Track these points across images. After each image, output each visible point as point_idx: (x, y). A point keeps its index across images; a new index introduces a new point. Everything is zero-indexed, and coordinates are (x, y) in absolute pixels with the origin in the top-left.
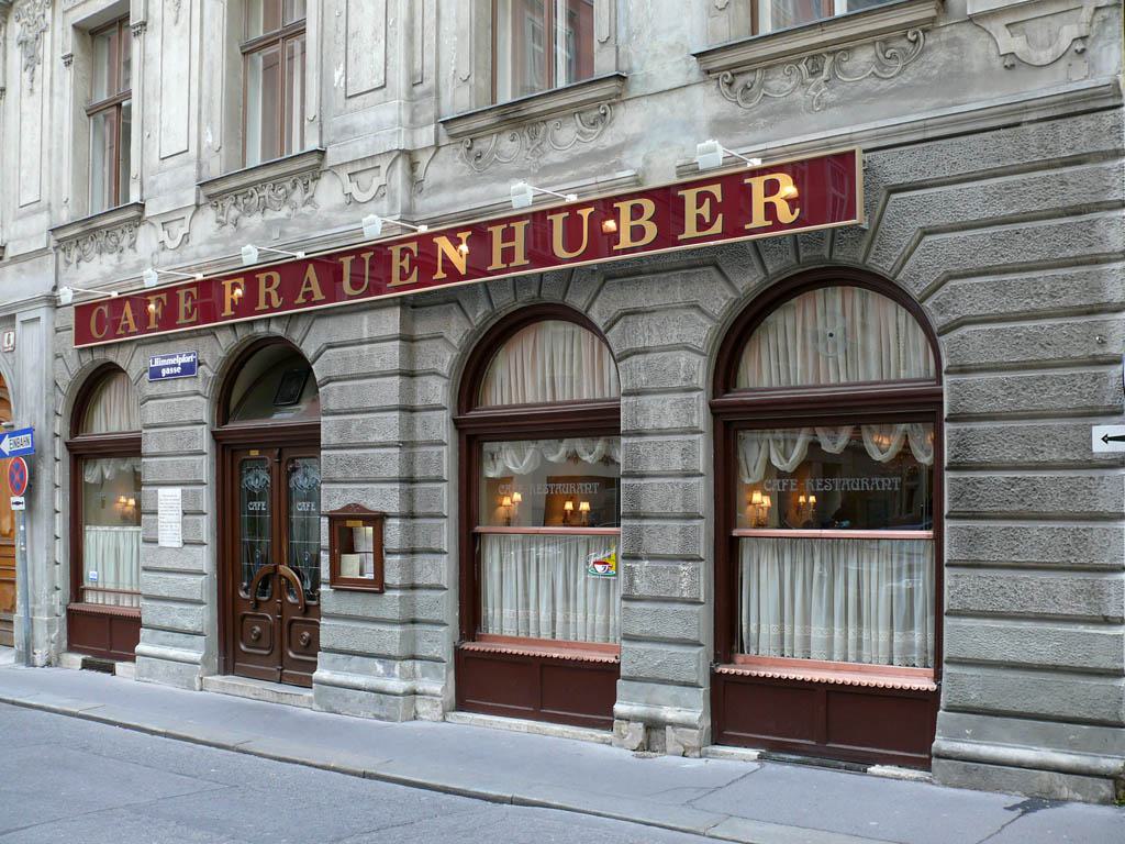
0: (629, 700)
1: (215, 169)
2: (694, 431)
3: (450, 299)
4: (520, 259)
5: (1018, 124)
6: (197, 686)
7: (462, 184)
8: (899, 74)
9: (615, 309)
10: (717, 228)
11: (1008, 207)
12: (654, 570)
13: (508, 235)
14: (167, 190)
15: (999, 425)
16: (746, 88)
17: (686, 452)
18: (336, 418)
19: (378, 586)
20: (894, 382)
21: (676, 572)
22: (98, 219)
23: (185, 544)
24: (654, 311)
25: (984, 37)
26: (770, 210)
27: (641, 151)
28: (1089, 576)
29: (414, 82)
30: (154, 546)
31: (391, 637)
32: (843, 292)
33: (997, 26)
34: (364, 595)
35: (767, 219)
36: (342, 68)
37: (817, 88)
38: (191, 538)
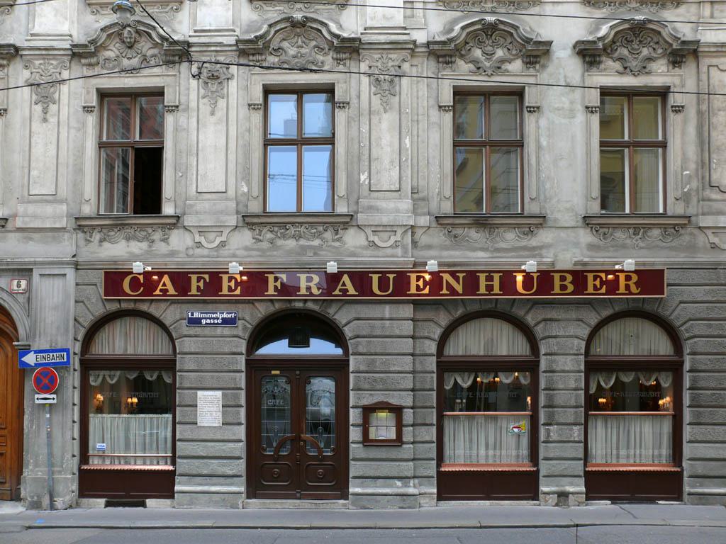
0: (547, 486)
1: (87, 210)
3: (589, 303)
4: (497, 290)
5: (716, 269)
6: (241, 506)
7: (446, 248)
8: (671, 242)
9: (540, 318)
10: (603, 290)
11: (713, 297)
12: (560, 430)
13: (490, 278)
14: (205, 212)
15: (708, 374)
17: (576, 380)
18: (364, 357)
19: (399, 441)
21: (571, 430)
22: (595, 219)
23: (223, 424)
24: (559, 320)
25: (703, 235)
26: (627, 287)
27: (552, 251)
29: (415, 191)
30: (195, 426)
31: (408, 468)
32: (625, 324)
33: (709, 232)
34: (388, 448)
36: (366, 174)
37: (637, 240)
38: (230, 420)
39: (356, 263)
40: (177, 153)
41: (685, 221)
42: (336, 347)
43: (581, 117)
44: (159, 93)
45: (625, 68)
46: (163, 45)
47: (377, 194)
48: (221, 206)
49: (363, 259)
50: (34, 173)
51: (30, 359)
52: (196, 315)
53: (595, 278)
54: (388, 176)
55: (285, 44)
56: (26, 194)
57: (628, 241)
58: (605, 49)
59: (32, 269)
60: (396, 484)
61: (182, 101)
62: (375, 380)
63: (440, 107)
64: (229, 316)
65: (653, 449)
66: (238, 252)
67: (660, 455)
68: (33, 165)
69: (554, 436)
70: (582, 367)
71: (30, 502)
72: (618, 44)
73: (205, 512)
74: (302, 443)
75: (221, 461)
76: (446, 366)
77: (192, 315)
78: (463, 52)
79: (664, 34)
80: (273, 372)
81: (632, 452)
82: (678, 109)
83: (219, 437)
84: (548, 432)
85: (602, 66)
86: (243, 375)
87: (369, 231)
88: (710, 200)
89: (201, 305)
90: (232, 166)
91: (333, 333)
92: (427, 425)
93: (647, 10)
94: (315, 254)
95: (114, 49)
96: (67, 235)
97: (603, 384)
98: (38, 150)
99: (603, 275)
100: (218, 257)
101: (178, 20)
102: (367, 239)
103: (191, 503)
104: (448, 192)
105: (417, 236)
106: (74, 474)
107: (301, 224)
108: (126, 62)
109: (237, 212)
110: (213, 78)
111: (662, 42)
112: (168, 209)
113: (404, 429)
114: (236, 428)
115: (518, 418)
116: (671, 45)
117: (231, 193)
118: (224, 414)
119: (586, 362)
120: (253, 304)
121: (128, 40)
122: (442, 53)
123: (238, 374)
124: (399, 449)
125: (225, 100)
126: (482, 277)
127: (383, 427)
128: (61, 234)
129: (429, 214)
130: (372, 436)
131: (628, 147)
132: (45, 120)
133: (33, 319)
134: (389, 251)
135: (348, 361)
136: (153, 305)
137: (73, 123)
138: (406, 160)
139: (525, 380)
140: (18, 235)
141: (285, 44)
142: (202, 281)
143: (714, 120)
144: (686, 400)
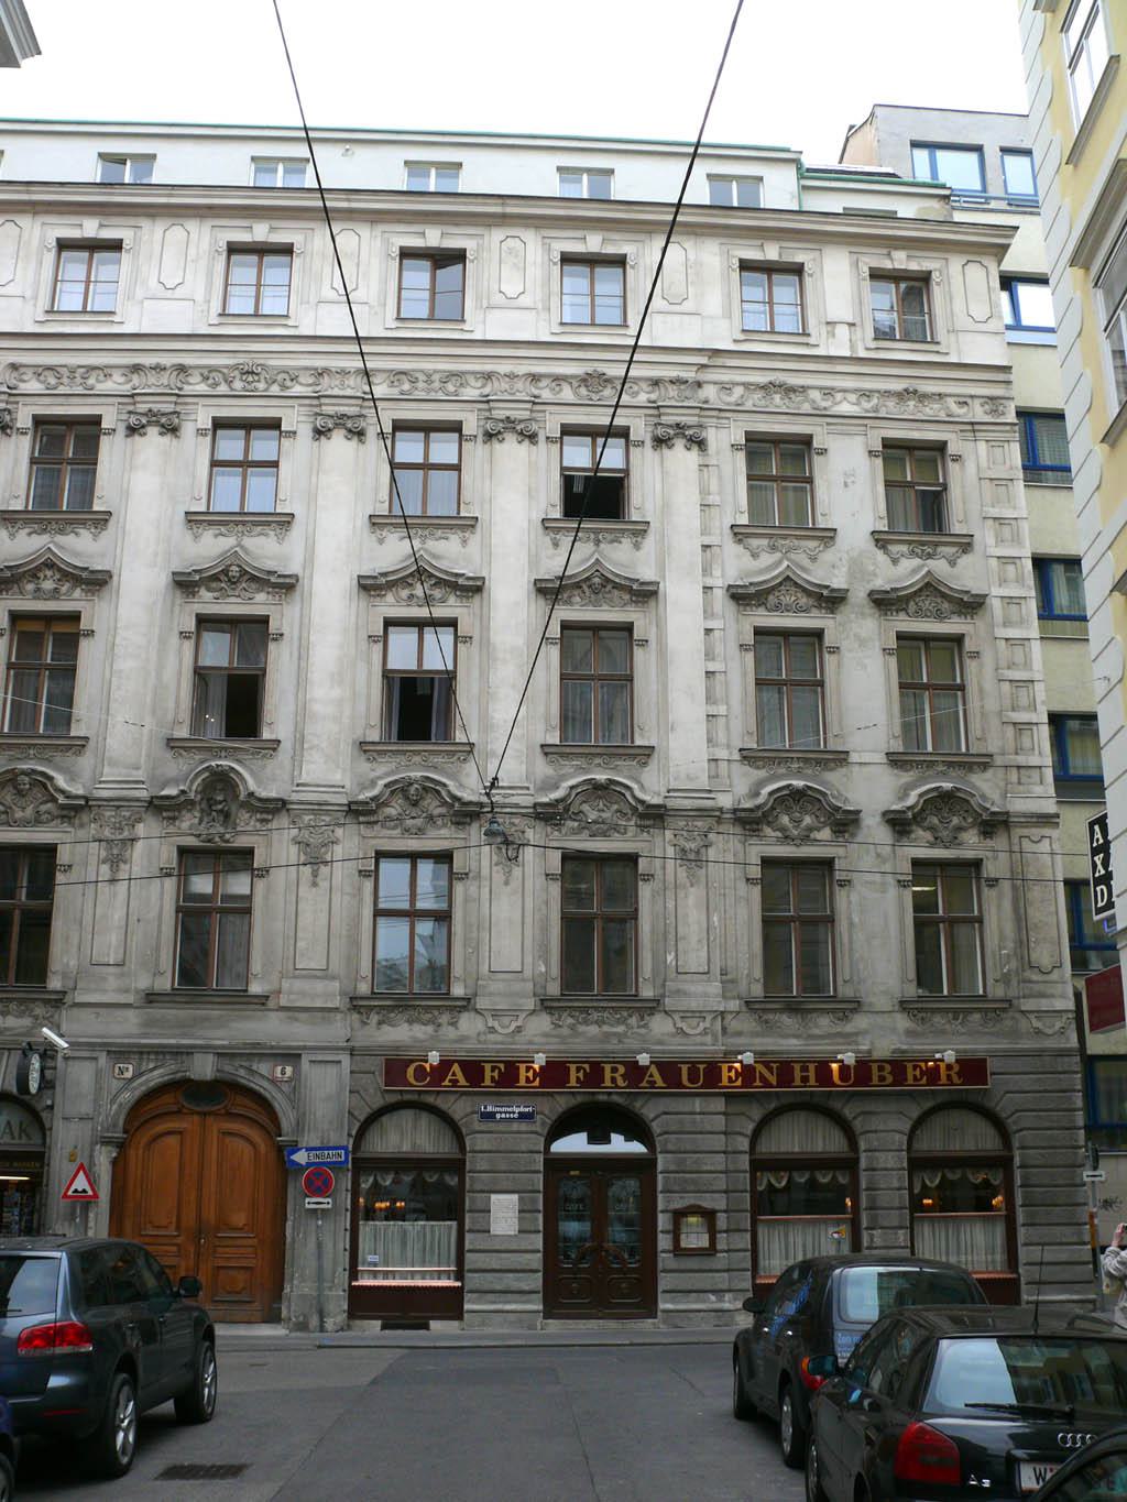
0: (666, 1302)
2: (904, 1169)
4: (812, 1081)
6: (539, 1327)
7: (757, 1035)
9: (858, 1110)
10: (739, 1083)
13: (805, 1069)
16: (922, 1019)
26: (613, 1080)
28: (1077, 1227)
29: (724, 972)
30: (487, 1234)
31: (721, 1280)
33: (1032, 1016)
36: (673, 954)
39: (663, 1052)
40: (467, 926)
41: (1005, 1005)
42: (626, 1140)
43: (893, 892)
44: (632, 859)
45: (936, 839)
46: (453, 806)
47: (685, 976)
48: (517, 987)
49: (518, 1047)
50: (300, 944)
51: (301, 1157)
52: (489, 1109)
53: (915, 1068)
54: (695, 958)
55: (585, 807)
56: (291, 967)
57: (947, 1026)
58: (914, 817)
59: (300, 1055)
60: (709, 1298)
61: (473, 868)
62: (686, 1181)
63: (748, 880)
64: (527, 1110)
65: (986, 1254)
66: (536, 1039)
67: (993, 1262)
68: (300, 934)
69: (878, 1241)
70: (905, 1165)
71: (295, 1324)
72: (927, 812)
73: (497, 1331)
74: (603, 1253)
75: (517, 1275)
76: (758, 1165)
77: (485, 1108)
78: (770, 819)
79: (972, 803)
80: (572, 1173)
81: (970, 1258)
82: (993, 882)
83: (515, 1247)
84: (872, 1236)
85: (913, 836)
86: (541, 1176)
87: (676, 1017)
88: (1030, 982)
89: (494, 1098)
90: (528, 943)
91: (635, 1128)
92: (740, 1231)
93: (954, 774)
94: (620, 1041)
95: (395, 805)
96: (339, 1016)
97: (928, 1182)
98: (306, 919)
99: (923, 1065)
100: (512, 1044)
101: (464, 773)
102: (675, 1024)
103: (483, 1324)
104: (758, 973)
105: (726, 1022)
107: (604, 1008)
108: (409, 822)
109: (535, 995)
110: (508, 845)
111: (971, 811)
112: (55, 983)
113: (718, 1235)
114: (533, 1236)
115: (838, 1222)
116: (981, 815)
117: (528, 973)
118: (520, 1219)
119: (751, 1162)
121: (415, 798)
122: (749, 821)
123: (535, 1175)
124: (712, 1258)
125: (521, 868)
126: (797, 1067)
127: (695, 1238)
128: (332, 1014)
129: (740, 998)
130: (683, 1245)
131: (943, 922)
132: (315, 884)
133: (301, 1110)
134: (699, 1039)
135: (656, 1159)
136: (441, 1096)
137: (348, 889)
138: (715, 939)
139: (843, 1179)
140: (281, 1014)
141: (585, 807)
142: (497, 1071)
143: (1029, 895)
144: (1019, 1201)
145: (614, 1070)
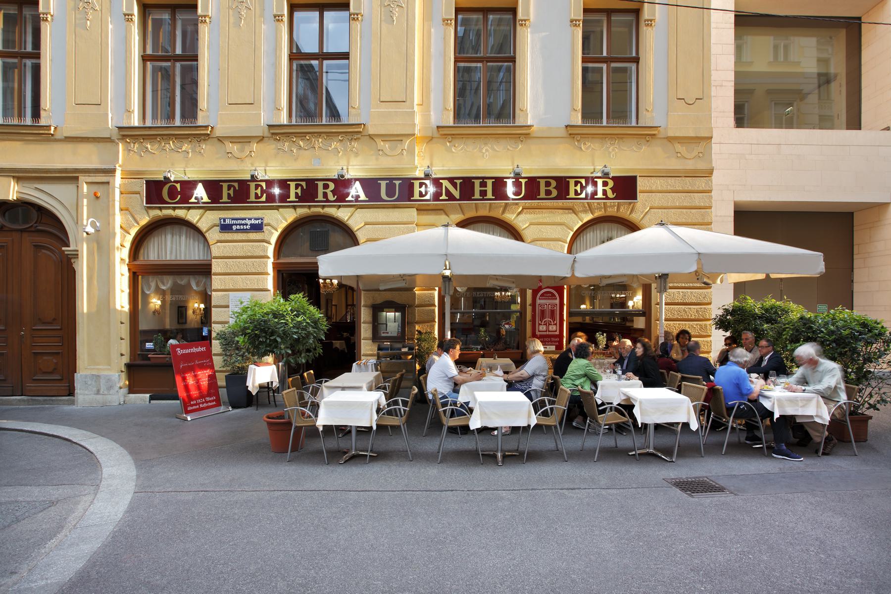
20: (146, 261)
26: (325, 195)
35: (603, 195)
106: (122, 372)
120: (295, 209)
145: (326, 187)
